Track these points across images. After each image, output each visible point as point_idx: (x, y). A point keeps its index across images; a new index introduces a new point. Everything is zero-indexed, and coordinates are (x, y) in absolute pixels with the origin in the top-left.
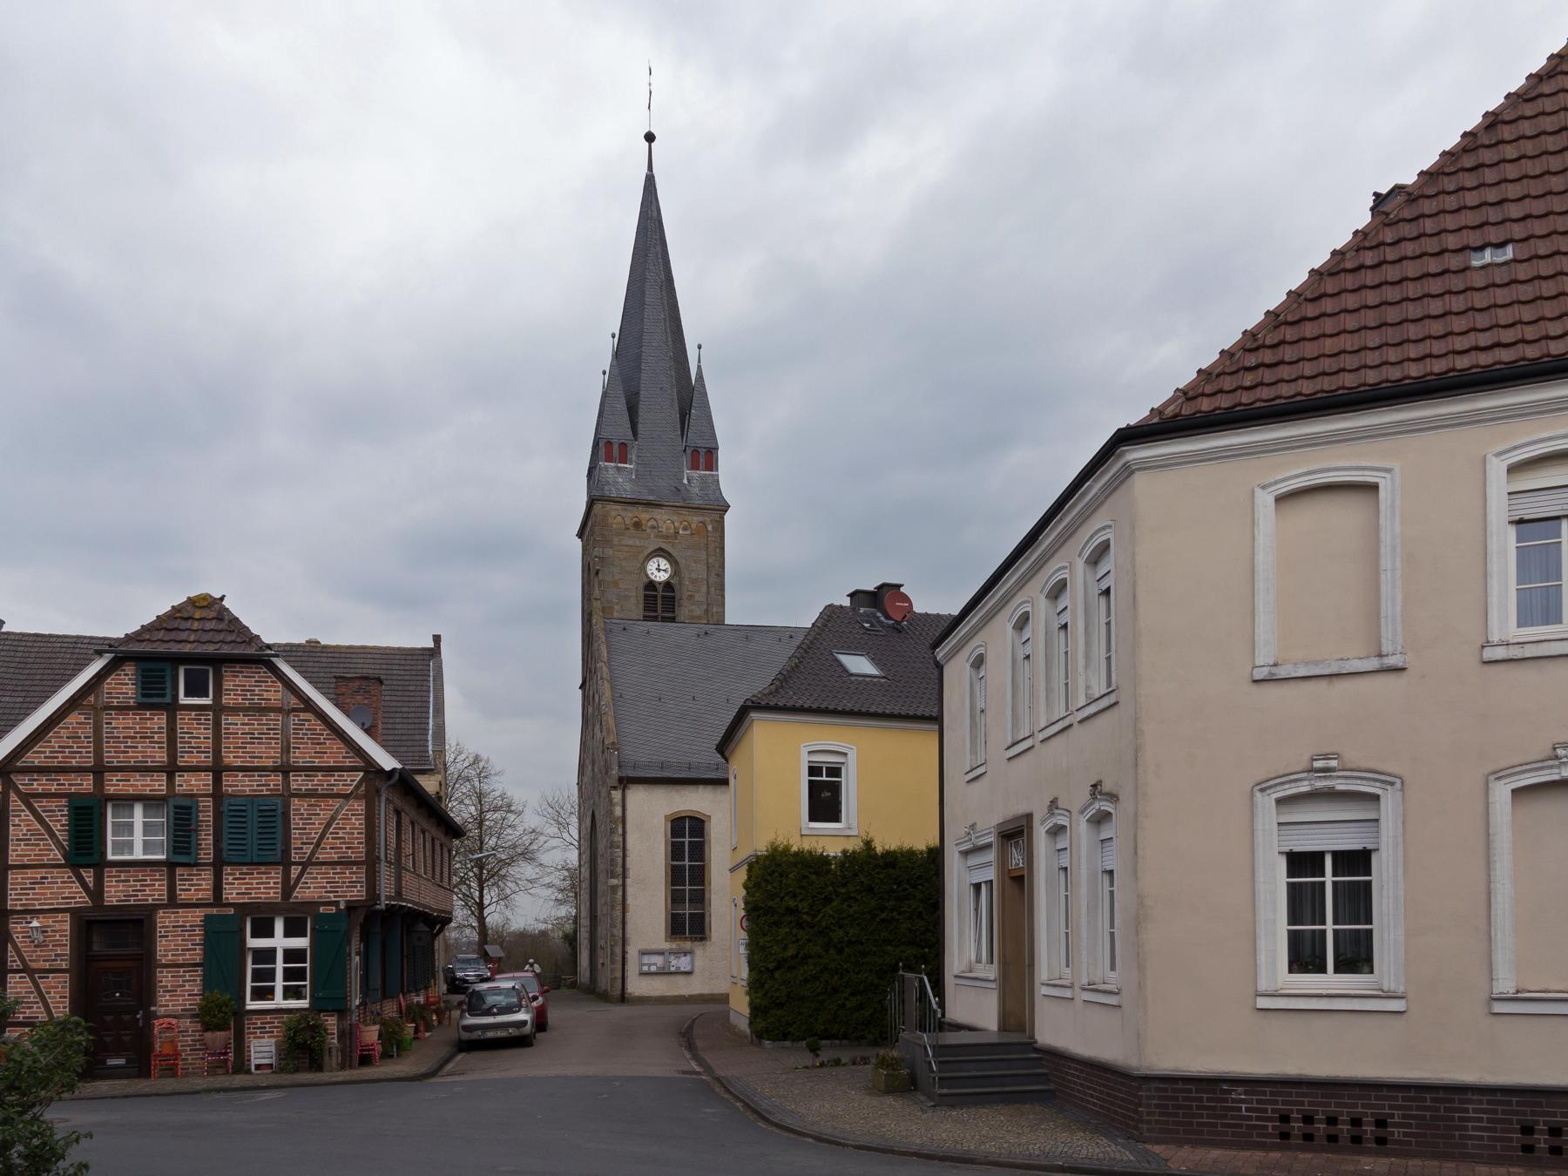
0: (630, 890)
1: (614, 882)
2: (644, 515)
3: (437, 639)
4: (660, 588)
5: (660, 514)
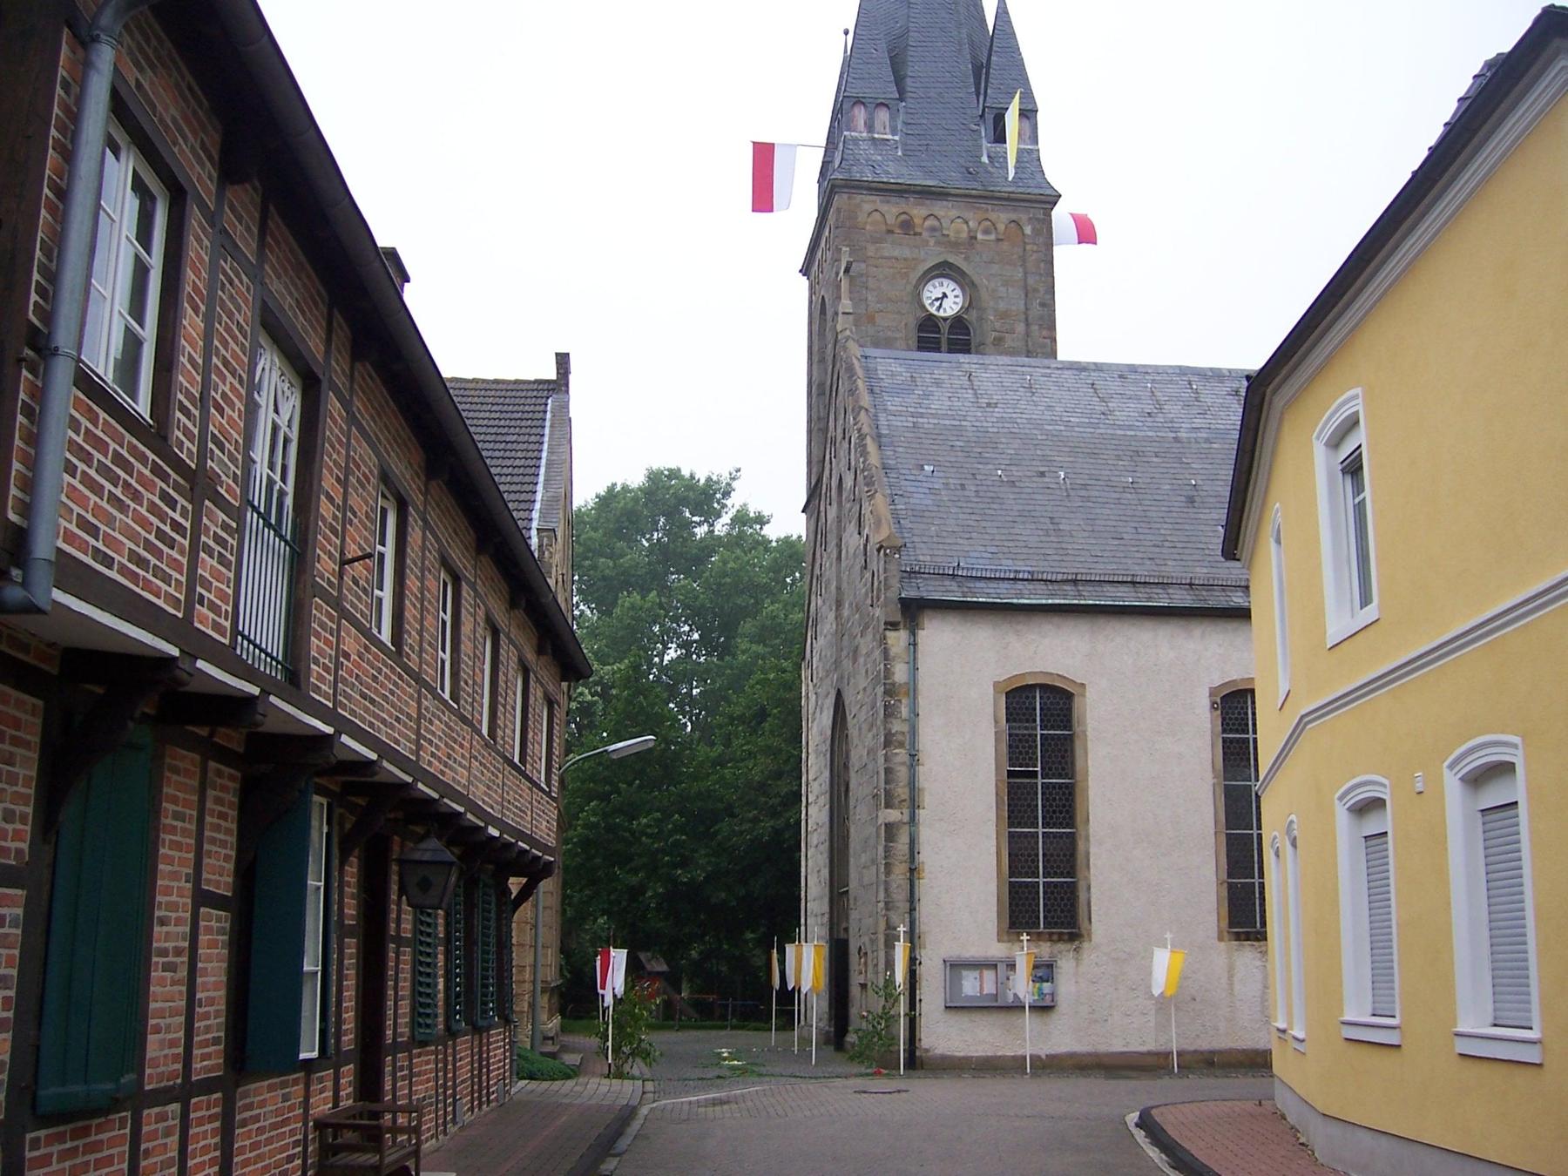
0: (926, 834)
1: (893, 815)
2: (918, 212)
3: (563, 361)
4: (945, 328)
5: (939, 208)
